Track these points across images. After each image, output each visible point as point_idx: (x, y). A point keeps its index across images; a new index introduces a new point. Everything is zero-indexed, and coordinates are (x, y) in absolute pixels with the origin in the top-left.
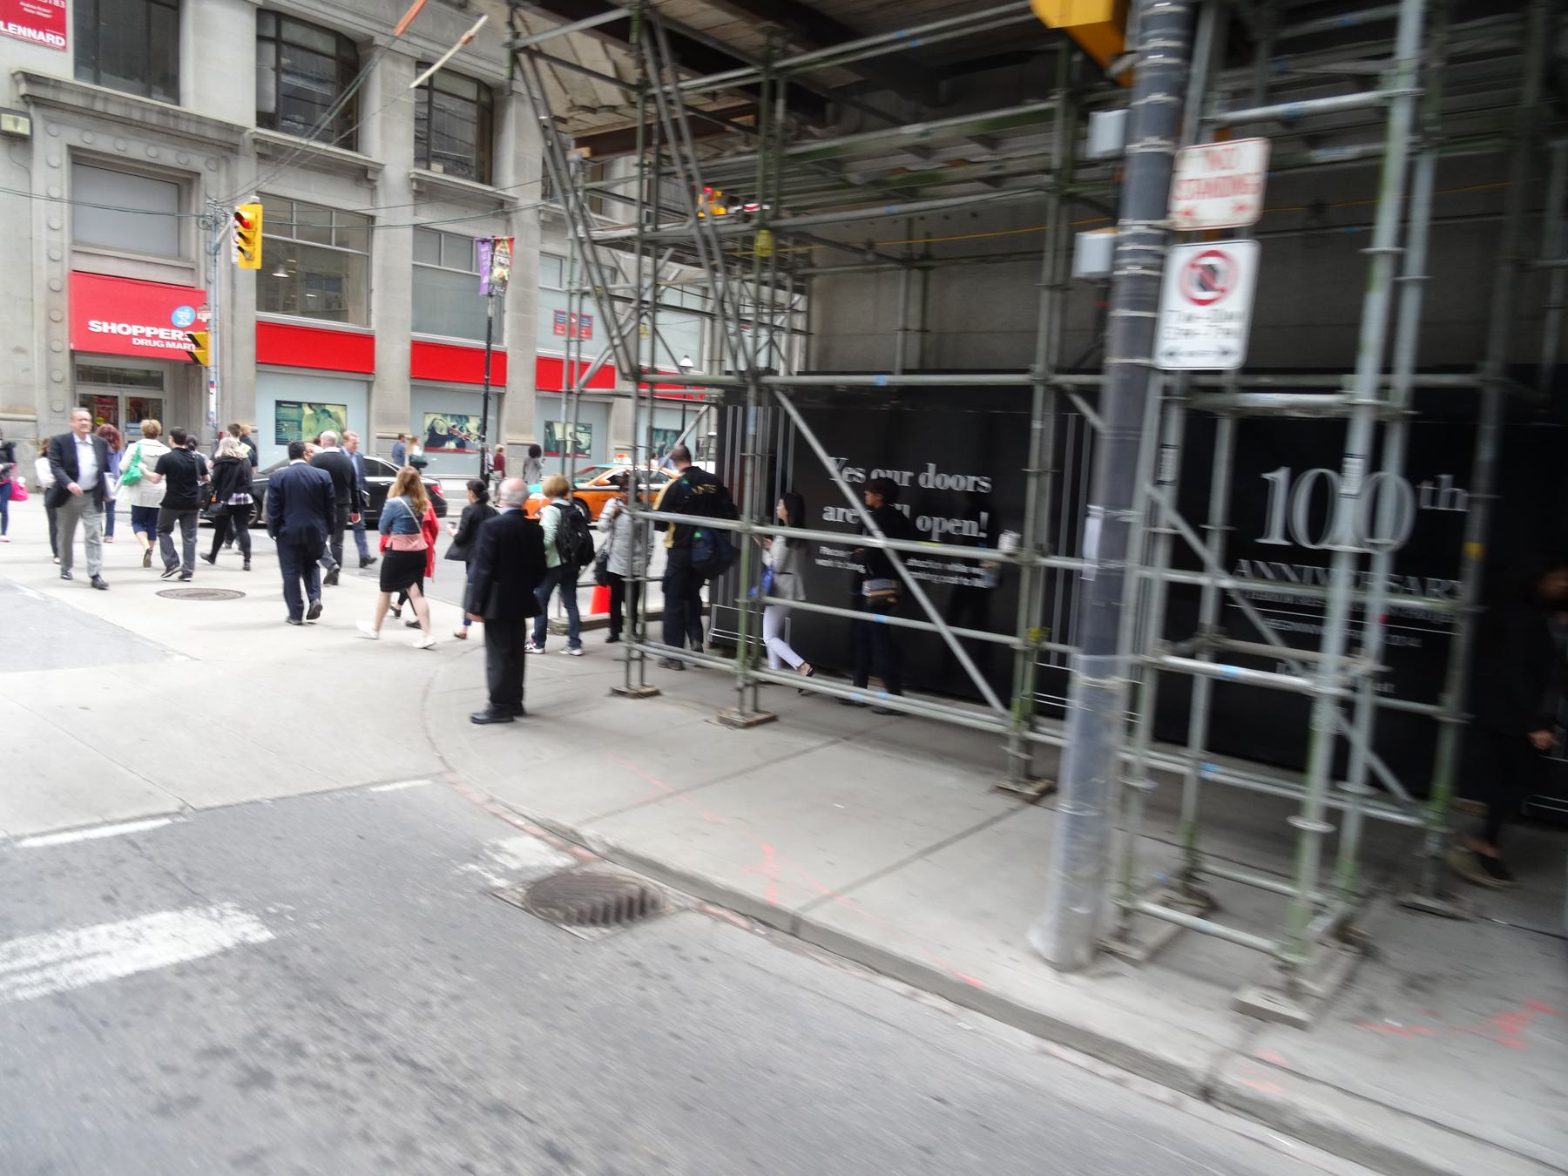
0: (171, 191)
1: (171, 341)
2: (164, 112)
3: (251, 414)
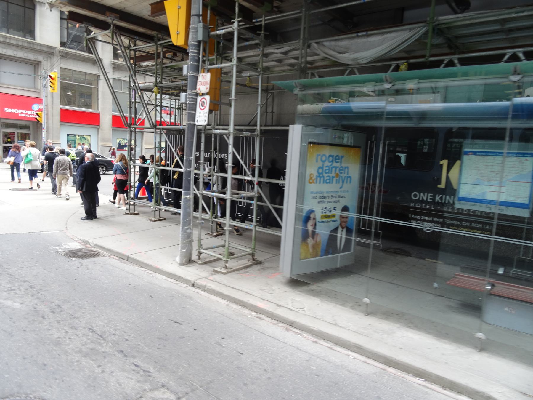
0: (33, 67)
1: (31, 115)
2: (29, 42)
3: (59, 138)
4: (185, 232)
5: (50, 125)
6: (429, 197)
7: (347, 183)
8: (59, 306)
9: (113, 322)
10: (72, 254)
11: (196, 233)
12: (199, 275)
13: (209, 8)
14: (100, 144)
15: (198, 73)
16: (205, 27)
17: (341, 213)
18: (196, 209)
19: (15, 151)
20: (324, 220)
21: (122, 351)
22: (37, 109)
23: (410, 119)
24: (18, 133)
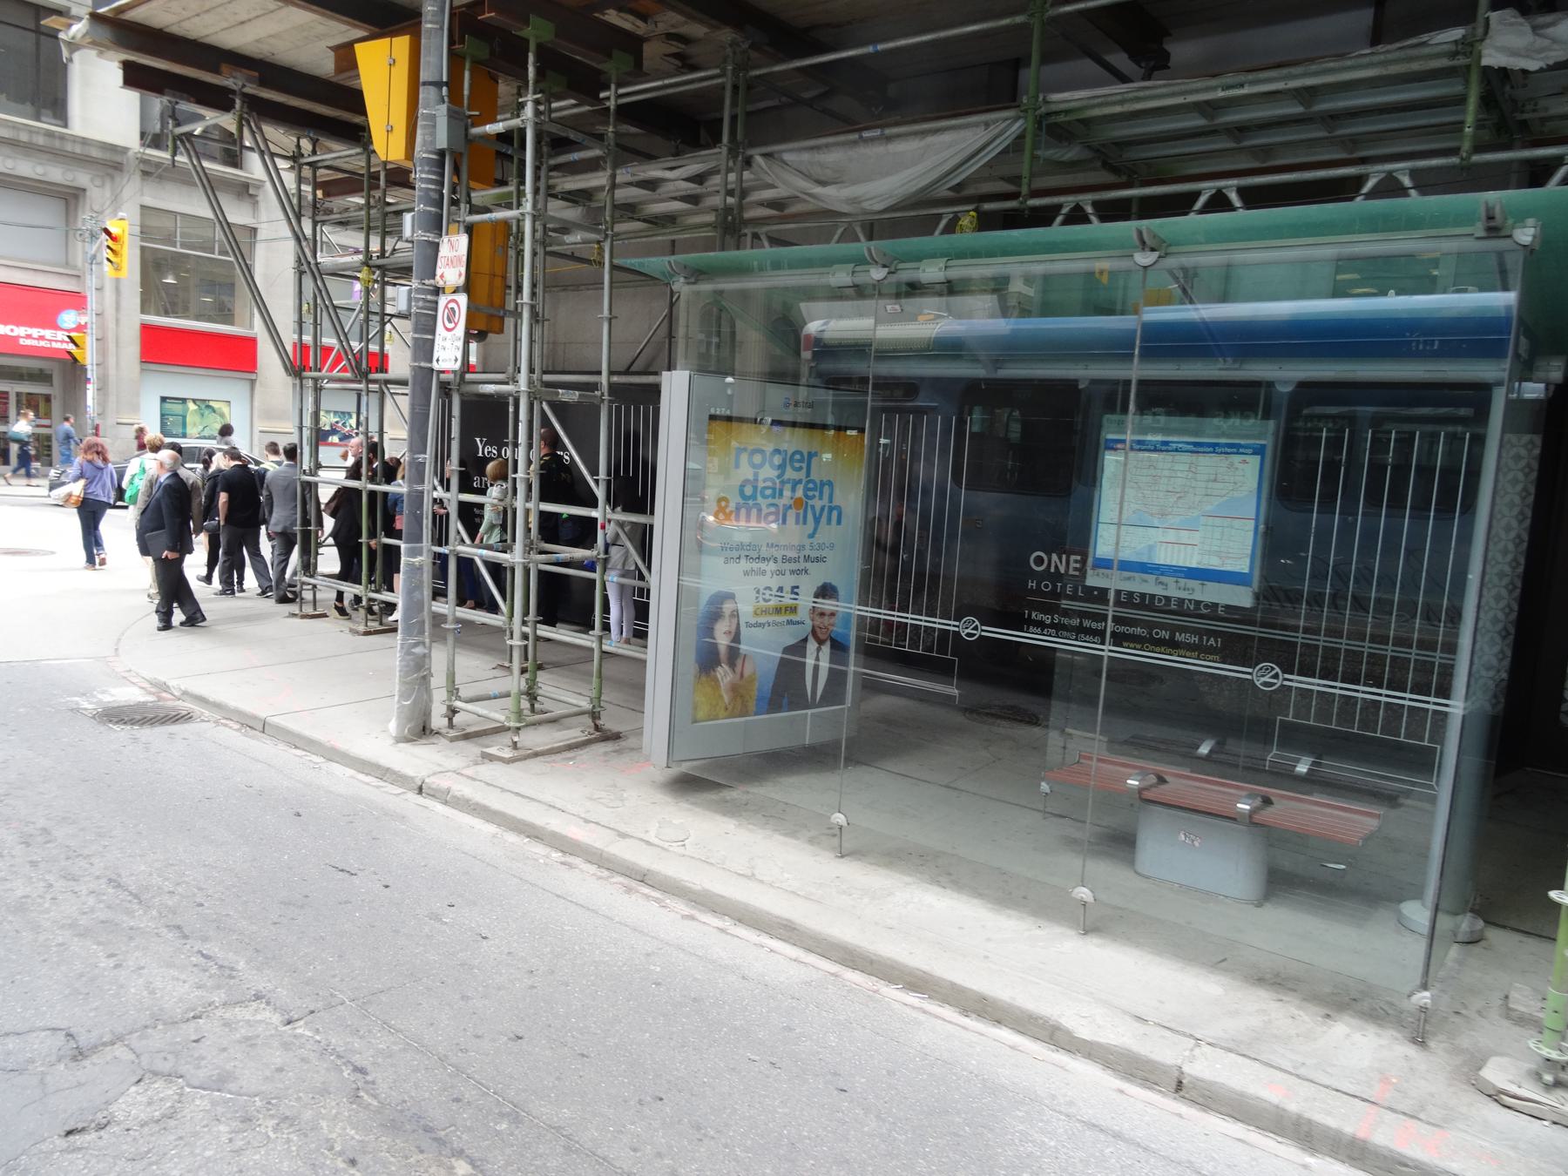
1: (56, 341)
2: (50, 134)
4: (408, 653)
5: (112, 372)
6: (1072, 565)
7: (829, 521)
8: (45, 831)
9: (176, 868)
10: (117, 716)
11: (439, 658)
12: (440, 765)
13: (467, 65)
14: (259, 426)
15: (441, 236)
16: (452, 115)
17: (814, 602)
18: (439, 594)
19: (90, 462)
20: (762, 620)
21: (179, 927)
22: (73, 326)
23: (975, 360)
24: (18, 394)
